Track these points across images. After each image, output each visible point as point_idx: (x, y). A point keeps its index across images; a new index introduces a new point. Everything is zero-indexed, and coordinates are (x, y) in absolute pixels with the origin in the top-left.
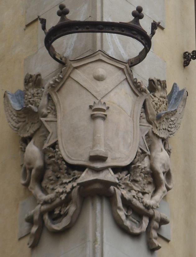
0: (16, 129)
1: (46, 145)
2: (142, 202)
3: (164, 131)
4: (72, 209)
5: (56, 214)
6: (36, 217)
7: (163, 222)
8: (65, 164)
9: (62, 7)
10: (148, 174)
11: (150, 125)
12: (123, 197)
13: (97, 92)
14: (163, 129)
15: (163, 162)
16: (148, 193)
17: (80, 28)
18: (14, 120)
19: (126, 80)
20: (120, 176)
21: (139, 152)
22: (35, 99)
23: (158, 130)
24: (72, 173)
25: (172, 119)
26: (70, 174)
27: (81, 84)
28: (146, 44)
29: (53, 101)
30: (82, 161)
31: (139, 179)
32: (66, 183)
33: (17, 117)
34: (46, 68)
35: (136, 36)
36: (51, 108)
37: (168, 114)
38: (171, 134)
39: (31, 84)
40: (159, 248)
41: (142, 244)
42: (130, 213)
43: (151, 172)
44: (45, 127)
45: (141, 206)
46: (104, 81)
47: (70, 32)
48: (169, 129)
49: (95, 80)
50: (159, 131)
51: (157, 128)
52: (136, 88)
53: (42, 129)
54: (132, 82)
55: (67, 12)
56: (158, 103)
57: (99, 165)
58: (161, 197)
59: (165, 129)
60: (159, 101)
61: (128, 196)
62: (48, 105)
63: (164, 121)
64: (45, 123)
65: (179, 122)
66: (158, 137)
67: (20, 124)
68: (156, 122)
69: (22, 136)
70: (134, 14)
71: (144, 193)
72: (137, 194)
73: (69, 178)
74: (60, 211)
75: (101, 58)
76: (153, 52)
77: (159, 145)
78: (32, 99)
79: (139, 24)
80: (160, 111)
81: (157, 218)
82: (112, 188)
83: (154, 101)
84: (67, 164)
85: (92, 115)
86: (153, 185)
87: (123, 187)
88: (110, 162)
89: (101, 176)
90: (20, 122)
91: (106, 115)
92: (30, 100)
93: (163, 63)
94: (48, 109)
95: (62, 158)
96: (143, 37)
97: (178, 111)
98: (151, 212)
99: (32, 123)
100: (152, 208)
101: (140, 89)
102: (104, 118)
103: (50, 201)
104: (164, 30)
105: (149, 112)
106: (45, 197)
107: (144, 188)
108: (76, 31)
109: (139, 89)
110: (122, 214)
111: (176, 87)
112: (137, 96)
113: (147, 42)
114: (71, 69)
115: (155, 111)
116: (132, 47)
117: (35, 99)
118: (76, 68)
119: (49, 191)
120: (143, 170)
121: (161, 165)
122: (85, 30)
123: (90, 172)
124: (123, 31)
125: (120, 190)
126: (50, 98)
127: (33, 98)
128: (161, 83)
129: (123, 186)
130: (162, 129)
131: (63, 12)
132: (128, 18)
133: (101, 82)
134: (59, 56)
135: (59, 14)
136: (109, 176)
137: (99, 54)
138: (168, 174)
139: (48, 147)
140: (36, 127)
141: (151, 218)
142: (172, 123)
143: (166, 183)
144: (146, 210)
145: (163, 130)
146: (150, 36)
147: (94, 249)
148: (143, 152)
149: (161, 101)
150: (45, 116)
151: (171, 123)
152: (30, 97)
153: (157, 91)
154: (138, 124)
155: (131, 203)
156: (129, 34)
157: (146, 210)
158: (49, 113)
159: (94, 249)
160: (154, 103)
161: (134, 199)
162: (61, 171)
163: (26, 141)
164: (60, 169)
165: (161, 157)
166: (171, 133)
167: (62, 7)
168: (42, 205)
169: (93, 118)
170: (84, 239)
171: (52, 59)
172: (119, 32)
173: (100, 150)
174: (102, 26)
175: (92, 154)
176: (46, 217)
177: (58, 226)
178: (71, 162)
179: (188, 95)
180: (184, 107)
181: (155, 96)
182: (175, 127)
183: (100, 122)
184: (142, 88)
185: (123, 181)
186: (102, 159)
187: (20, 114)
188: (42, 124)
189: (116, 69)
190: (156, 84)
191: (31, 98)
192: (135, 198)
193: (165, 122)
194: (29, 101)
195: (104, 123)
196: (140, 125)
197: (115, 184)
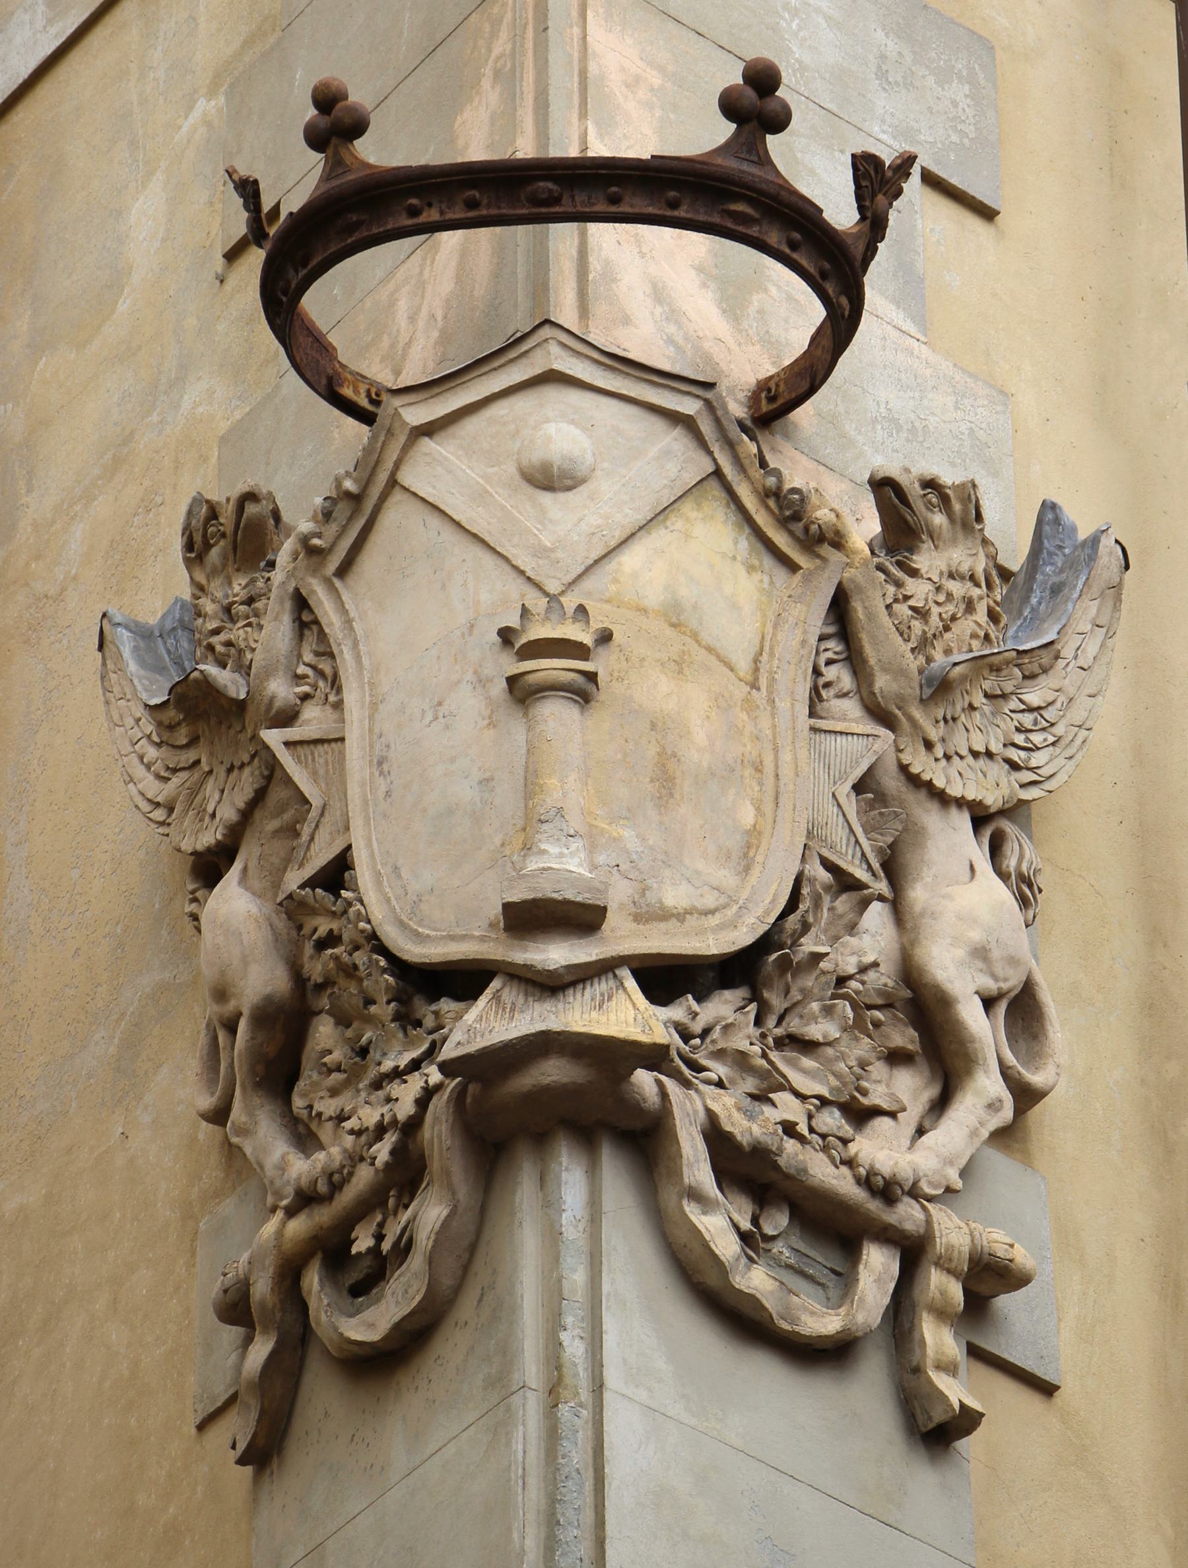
0: (160, 814)
1: (293, 880)
2: (850, 1163)
3: (982, 762)
4: (429, 1213)
5: (359, 1254)
6: (262, 1288)
7: (989, 1279)
8: (384, 971)
9: (327, 99)
10: (887, 1006)
11: (882, 731)
12: (717, 1138)
13: (541, 552)
14: (975, 754)
15: (976, 935)
16: (892, 1115)
17: (430, 205)
18: (148, 767)
19: (714, 484)
20: (695, 1015)
21: (812, 881)
22: (237, 633)
23: (936, 760)
24: (426, 1012)
25: (1033, 697)
26: (418, 1024)
27: (455, 517)
28: (824, 275)
29: (322, 636)
30: (473, 937)
31: (816, 1031)
32: (397, 1074)
33: (159, 745)
34: (306, 460)
35: (754, 231)
36: (314, 667)
37: (996, 669)
38: (1034, 783)
39: (214, 554)
40: (967, 1421)
41: (868, 1389)
42: (777, 1222)
43: (908, 994)
44: (288, 781)
45: (842, 1183)
46: (583, 490)
47: (375, 230)
48: (1015, 755)
49: (530, 490)
50: (944, 762)
51: (929, 745)
52: (790, 529)
53: (277, 794)
54: (755, 491)
55: (356, 127)
56: (935, 610)
57: (556, 954)
58: (974, 1133)
59: (989, 754)
60: (941, 598)
61: (747, 1126)
62: (300, 656)
63: (972, 708)
64: (285, 758)
65: (1077, 714)
66: (942, 798)
67: (176, 780)
68: (917, 714)
69: (187, 845)
70: (730, 106)
71: (861, 1115)
72: (810, 1117)
73: (410, 1043)
74: (379, 1237)
75: (557, 366)
76: (923, 339)
77: (951, 843)
78: (223, 637)
79: (765, 160)
80: (948, 652)
81: (950, 1247)
82: (644, 1080)
83: (907, 598)
84: (398, 965)
85: (512, 681)
86: (927, 1072)
87: (713, 1076)
88: (623, 937)
89: (579, 1015)
90: (175, 771)
91: (592, 677)
92: (215, 640)
93: (936, 382)
94: (298, 678)
95: (373, 936)
96: (797, 236)
97: (1067, 652)
98: (908, 1215)
99: (230, 770)
100: (914, 1193)
101: (806, 529)
102: (583, 692)
103: (322, 1188)
104: (998, 218)
105: (869, 650)
106: (301, 1168)
107: (864, 1084)
108: (409, 222)
109: (798, 527)
110: (718, 1226)
111: (1057, 521)
112: (793, 567)
113: (827, 266)
114: (402, 439)
115: (913, 650)
116: (766, 312)
117: (237, 633)
118: (429, 430)
119: (325, 1132)
120: (854, 984)
121: (961, 953)
122: (458, 216)
123: (511, 994)
124: (674, 205)
125: (697, 1090)
126: (306, 617)
127: (229, 625)
128: (945, 500)
129: (719, 1070)
130: (964, 752)
131: (334, 124)
132: (704, 134)
133: (562, 496)
134: (363, 389)
135: (316, 139)
136: (623, 1014)
137: (546, 340)
138: (1022, 1010)
139: (302, 886)
140: (246, 785)
141: (913, 1252)
142: (1036, 723)
143: (1010, 1058)
144: (874, 1206)
145: (970, 759)
146: (857, 236)
147: (552, 1435)
148: (844, 883)
149: (950, 596)
150: (287, 718)
151: (1027, 720)
152: (212, 625)
153: (927, 545)
154: (804, 721)
155: (776, 1167)
156: (716, 219)
157: (874, 1206)
158: (305, 697)
159: (552, 1435)
160: (903, 610)
161: (790, 1145)
162: (373, 1009)
163: (209, 868)
164: (369, 1001)
165: (962, 915)
166: (1027, 776)
167: (327, 99)
168: (291, 1212)
169: (522, 692)
170: (502, 1384)
171: (324, 404)
172: (651, 210)
173: (563, 865)
174: (550, 185)
175: (517, 895)
176: (312, 1279)
177: (369, 1325)
178: (414, 951)
179: (1127, 567)
180: (1110, 635)
181: (914, 573)
182: (1053, 744)
183: (556, 714)
184: (813, 522)
185: (713, 1042)
186: (581, 919)
187: (171, 728)
188: (272, 771)
189: (658, 424)
190: (918, 505)
191: (216, 632)
192: (801, 1139)
193: (983, 715)
194: (211, 648)
195: (587, 727)
196: (814, 729)
197: (655, 1057)
